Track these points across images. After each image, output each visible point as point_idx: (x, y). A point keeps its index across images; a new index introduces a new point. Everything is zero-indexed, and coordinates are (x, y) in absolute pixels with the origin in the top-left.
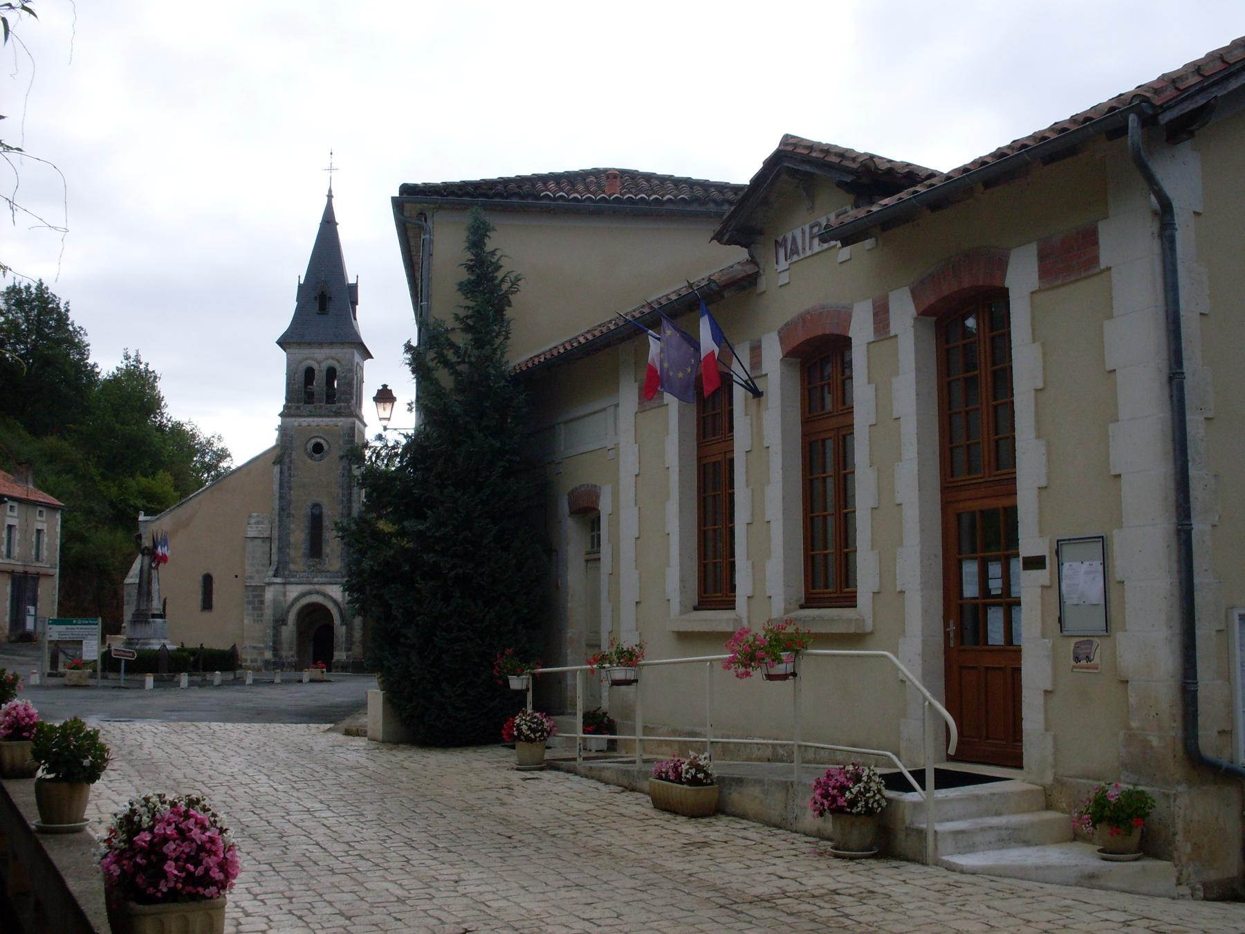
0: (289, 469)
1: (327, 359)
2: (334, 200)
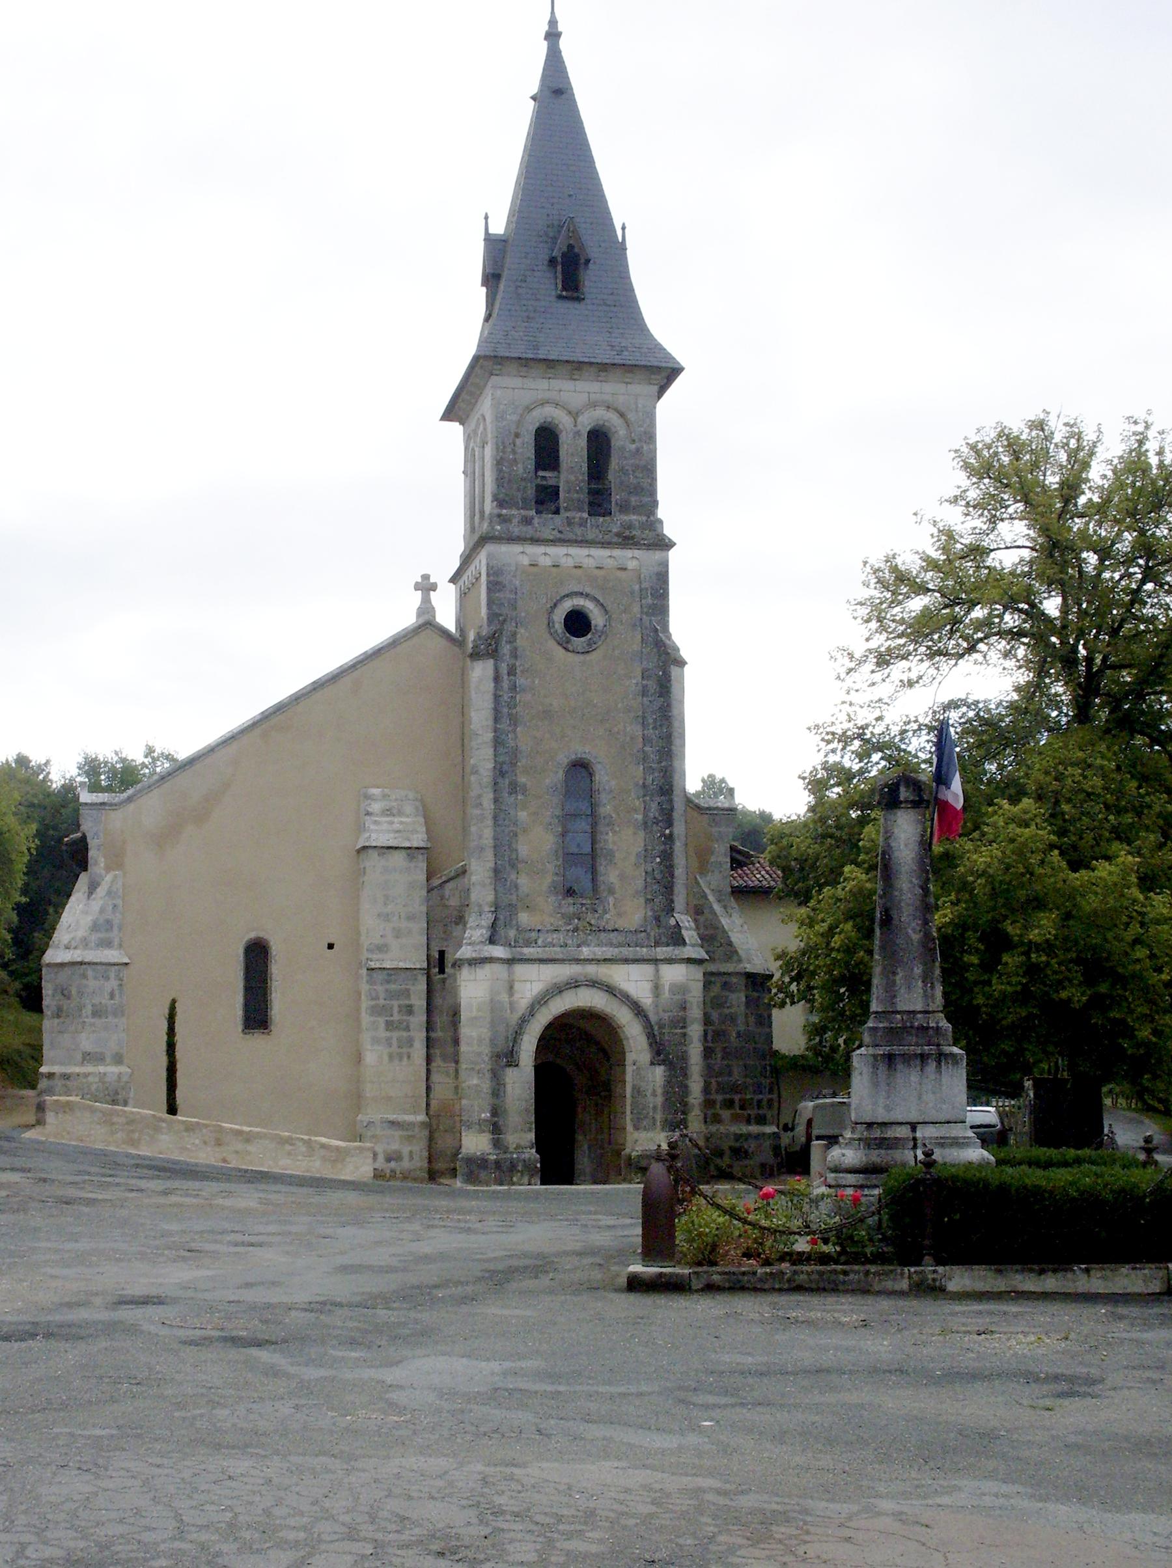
0: (512, 672)
1: (594, 405)
2: (563, 44)
